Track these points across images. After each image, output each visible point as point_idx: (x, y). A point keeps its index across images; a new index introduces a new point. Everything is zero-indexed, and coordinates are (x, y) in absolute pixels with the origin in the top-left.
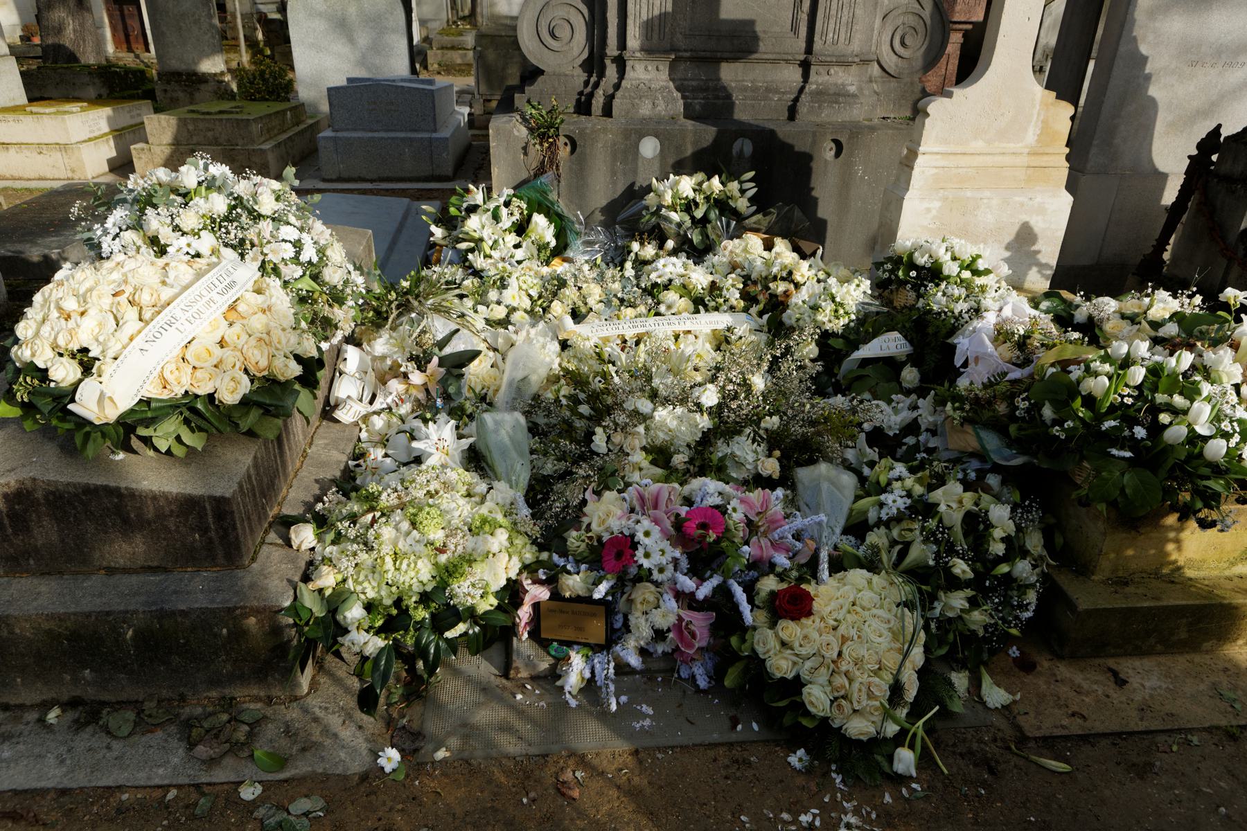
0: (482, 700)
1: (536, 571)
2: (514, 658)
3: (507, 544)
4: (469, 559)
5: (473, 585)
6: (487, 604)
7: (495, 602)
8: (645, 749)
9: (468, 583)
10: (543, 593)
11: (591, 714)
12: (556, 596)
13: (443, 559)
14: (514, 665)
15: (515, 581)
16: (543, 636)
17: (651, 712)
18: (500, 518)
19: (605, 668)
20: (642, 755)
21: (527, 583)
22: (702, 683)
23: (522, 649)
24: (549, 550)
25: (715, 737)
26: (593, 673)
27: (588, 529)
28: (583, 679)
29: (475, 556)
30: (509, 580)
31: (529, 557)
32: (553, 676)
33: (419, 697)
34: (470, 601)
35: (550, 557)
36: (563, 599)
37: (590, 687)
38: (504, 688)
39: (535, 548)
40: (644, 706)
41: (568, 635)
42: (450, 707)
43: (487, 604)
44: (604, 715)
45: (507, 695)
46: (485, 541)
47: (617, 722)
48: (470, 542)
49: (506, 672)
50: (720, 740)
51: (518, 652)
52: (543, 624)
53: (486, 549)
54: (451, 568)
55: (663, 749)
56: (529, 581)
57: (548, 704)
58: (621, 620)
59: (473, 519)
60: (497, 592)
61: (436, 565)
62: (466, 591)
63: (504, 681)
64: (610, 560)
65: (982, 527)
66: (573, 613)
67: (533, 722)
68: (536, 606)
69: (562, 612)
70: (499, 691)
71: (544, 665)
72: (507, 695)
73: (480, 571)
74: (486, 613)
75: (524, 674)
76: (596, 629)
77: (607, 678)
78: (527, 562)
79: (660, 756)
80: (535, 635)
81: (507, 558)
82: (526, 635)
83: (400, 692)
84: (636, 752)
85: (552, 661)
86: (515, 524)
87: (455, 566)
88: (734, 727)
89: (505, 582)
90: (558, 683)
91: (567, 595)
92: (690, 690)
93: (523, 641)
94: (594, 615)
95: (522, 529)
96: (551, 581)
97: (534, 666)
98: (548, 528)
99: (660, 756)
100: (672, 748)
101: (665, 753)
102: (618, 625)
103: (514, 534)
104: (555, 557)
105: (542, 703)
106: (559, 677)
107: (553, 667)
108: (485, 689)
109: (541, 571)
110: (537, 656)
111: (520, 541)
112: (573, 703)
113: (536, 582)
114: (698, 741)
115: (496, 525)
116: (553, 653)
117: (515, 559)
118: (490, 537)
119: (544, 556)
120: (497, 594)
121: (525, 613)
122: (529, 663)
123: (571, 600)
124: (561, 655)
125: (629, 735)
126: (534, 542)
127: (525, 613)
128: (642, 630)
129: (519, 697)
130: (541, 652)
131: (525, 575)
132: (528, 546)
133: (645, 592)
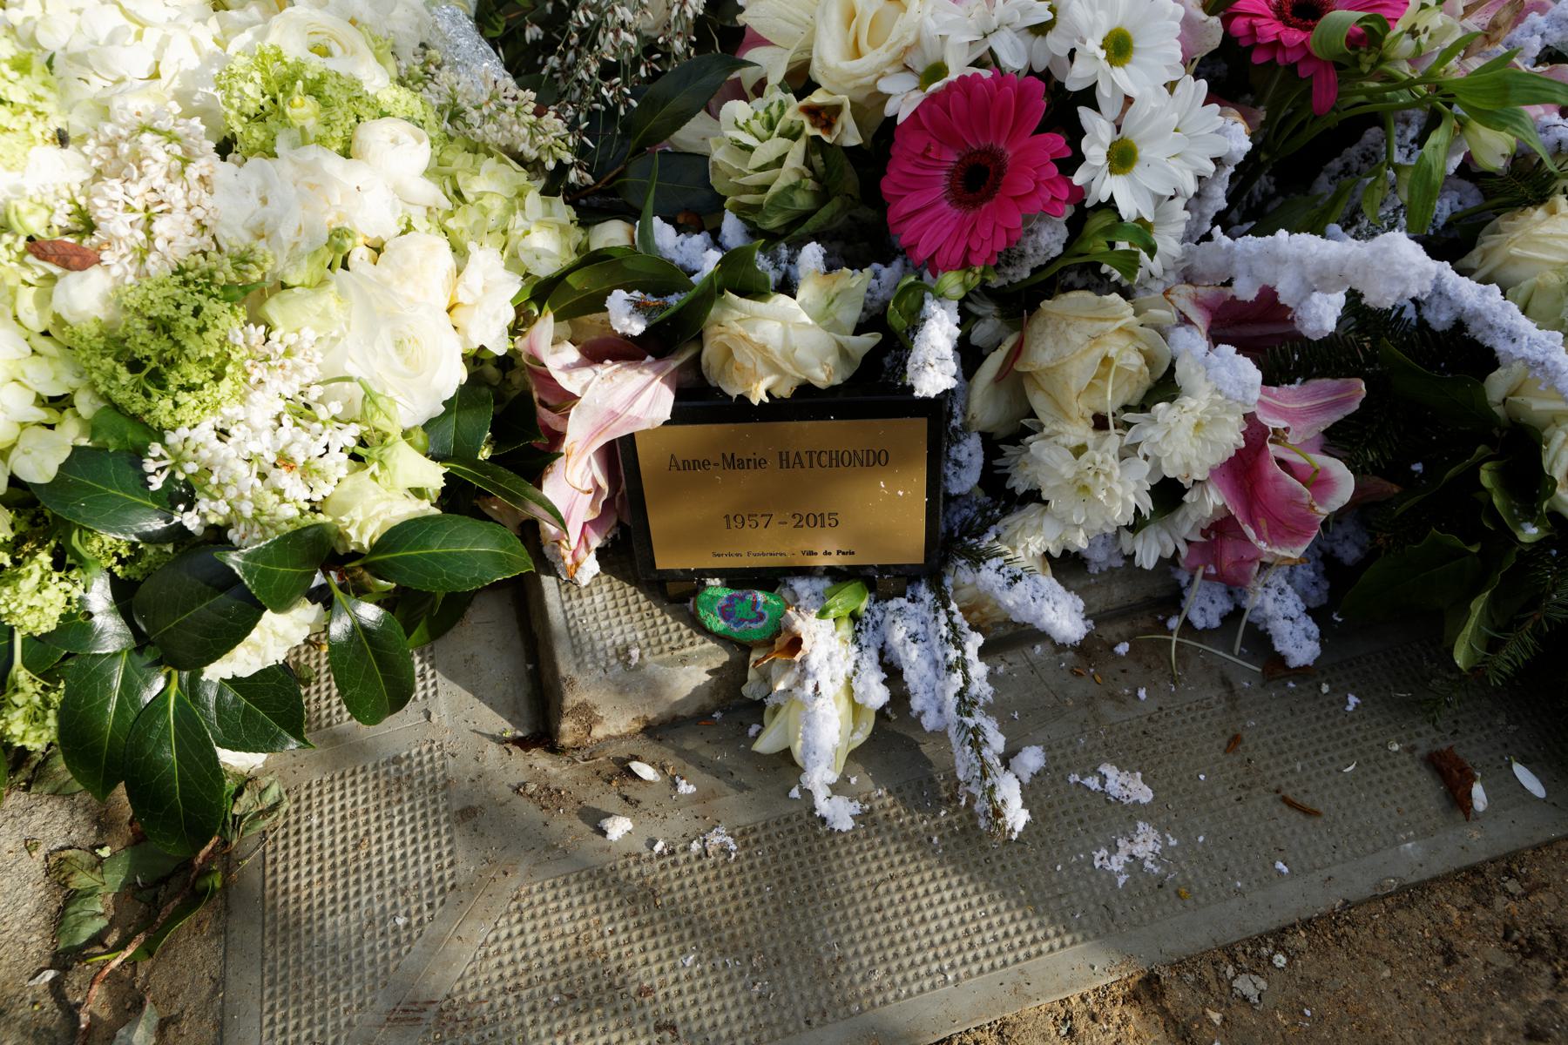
0: (466, 867)
1: (597, 303)
2: (565, 666)
3: (431, 193)
4: (232, 282)
5: (304, 412)
6: (392, 495)
7: (433, 476)
8: (1178, 965)
9: (265, 405)
10: (638, 399)
11: (918, 843)
12: (699, 399)
13: (86, 297)
14: (570, 700)
15: (507, 362)
16: (663, 562)
17: (1145, 795)
18: (376, 80)
19: (948, 672)
20: (1177, 995)
21: (560, 361)
22: (1298, 642)
23: (589, 626)
24: (630, 214)
25: (1412, 856)
26: (892, 673)
27: (801, 81)
28: (857, 709)
29: (272, 261)
30: (475, 360)
31: (548, 240)
32: (731, 721)
33: (195, 897)
34: (290, 503)
35: (646, 235)
36: (742, 410)
37: (892, 741)
38: (550, 795)
39: (563, 211)
40: (1109, 770)
41: (762, 546)
42: (337, 924)
43: (392, 495)
44: (970, 842)
45: (565, 824)
46: (316, 185)
47: (1042, 875)
48: (232, 196)
49: (540, 719)
50: (1438, 867)
51: (573, 636)
52: (659, 521)
53: (330, 220)
54: (146, 345)
55: (1248, 952)
56: (571, 354)
57: (742, 835)
58: (978, 460)
59: (225, 83)
60: (429, 426)
61: (55, 333)
62: (265, 446)
63: (540, 760)
64: (925, 207)
65: (1050, 239)
66: (784, 460)
67: (687, 924)
68: (619, 456)
69: (733, 462)
70: (528, 810)
71: (691, 674)
72: (565, 824)
73: (314, 334)
74: (396, 536)
75: (619, 723)
76: (891, 509)
77: (966, 702)
78: (545, 269)
79: (1245, 985)
80: (626, 550)
81: (447, 259)
82: (590, 567)
83: (114, 879)
84: (1148, 990)
85: (721, 657)
86: (455, 114)
87: (162, 327)
88: (1459, 801)
89: (460, 374)
90: (766, 743)
91: (758, 395)
92: (1247, 672)
93: (586, 598)
94: (877, 460)
95: (491, 133)
96: (672, 339)
97: (653, 688)
98: (602, 120)
99: (1245, 985)
100: (1279, 935)
101: (1260, 966)
102: (966, 479)
103: (459, 160)
104: (664, 235)
105: (716, 839)
106: (756, 711)
107: (729, 680)
108: (469, 812)
109: (618, 301)
110: (654, 644)
111: (491, 183)
112: (840, 813)
113: (605, 350)
114: (1360, 885)
115: (344, 121)
116: (718, 624)
117: (487, 262)
118: (333, 163)
119: (612, 234)
120: (439, 437)
121: (572, 487)
122: (627, 674)
123: (775, 409)
124: (756, 630)
125: (1094, 913)
126: (555, 183)
127: (572, 487)
128: (1091, 489)
129: (619, 827)
130: (667, 624)
131: (546, 327)
132: (533, 198)
133: (1087, 343)
